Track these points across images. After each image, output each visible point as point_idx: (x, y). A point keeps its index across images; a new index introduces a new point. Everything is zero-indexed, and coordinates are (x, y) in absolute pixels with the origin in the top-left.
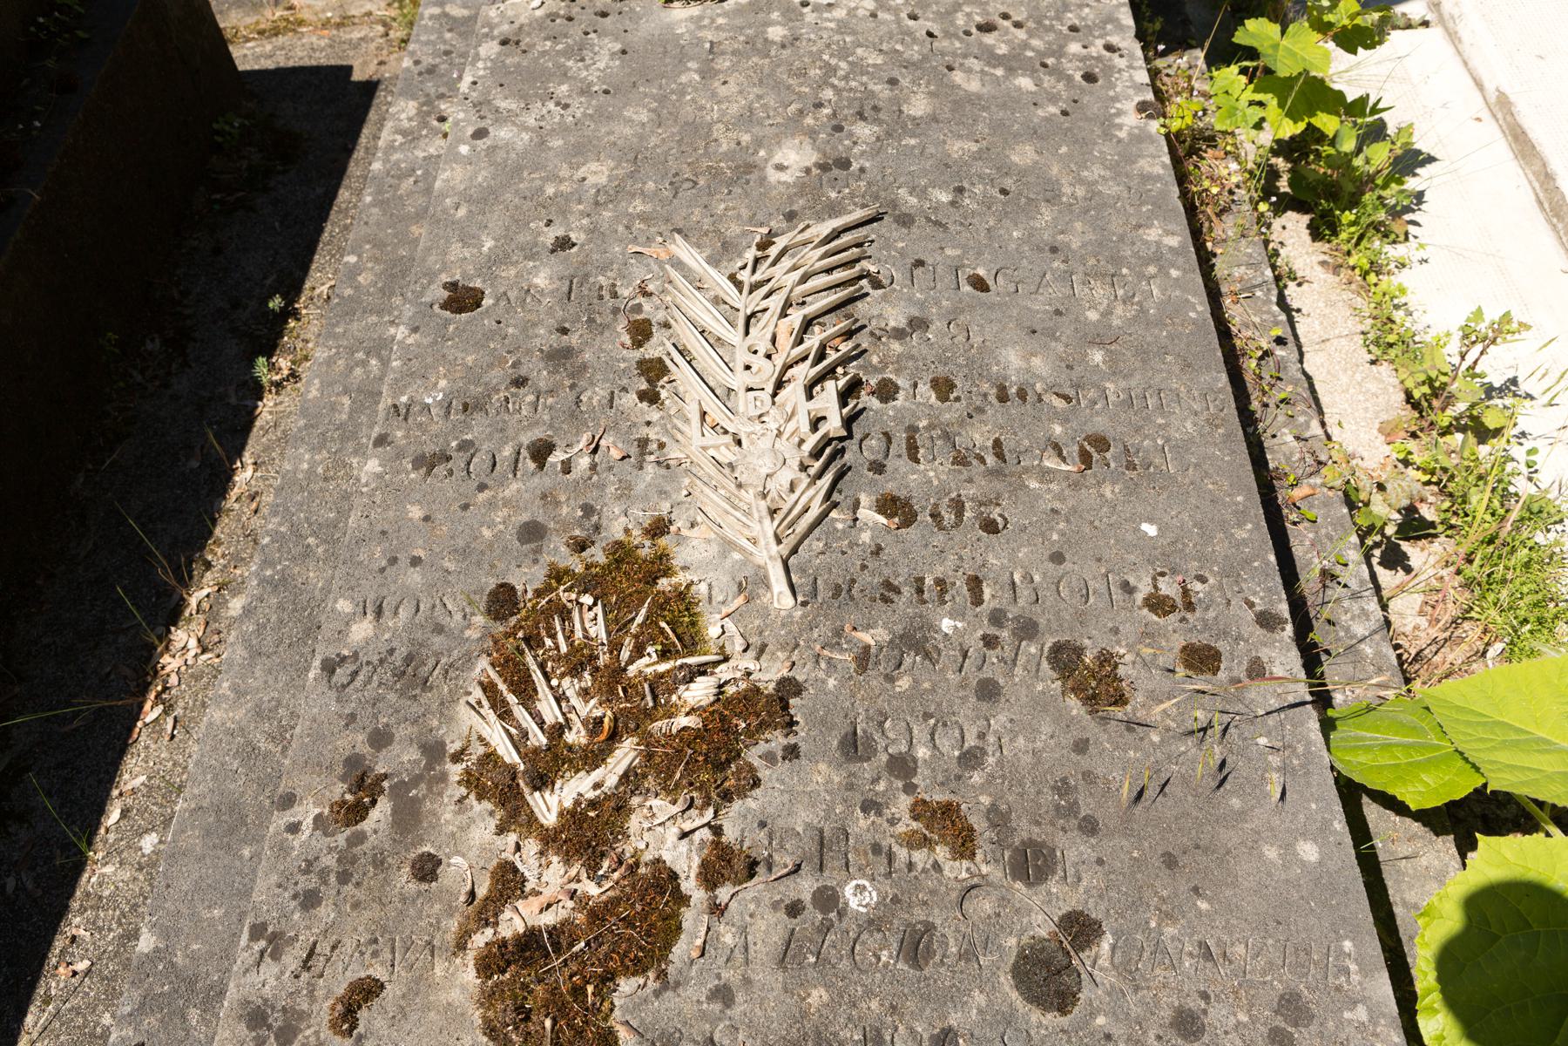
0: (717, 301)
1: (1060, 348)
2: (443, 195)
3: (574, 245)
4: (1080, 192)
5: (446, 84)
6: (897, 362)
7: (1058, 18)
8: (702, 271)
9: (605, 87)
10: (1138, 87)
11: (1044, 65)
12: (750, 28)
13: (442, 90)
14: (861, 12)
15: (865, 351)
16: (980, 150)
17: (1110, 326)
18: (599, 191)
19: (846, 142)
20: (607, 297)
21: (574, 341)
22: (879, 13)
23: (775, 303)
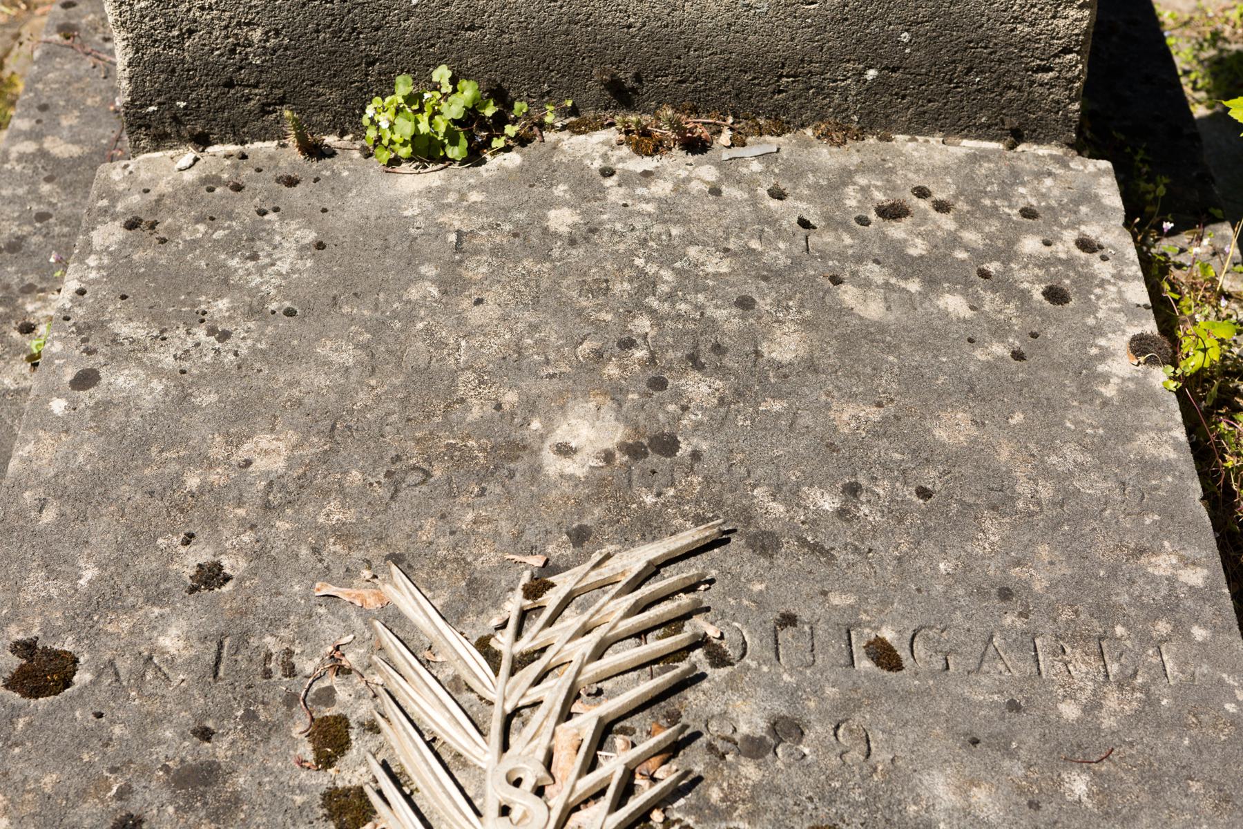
0: (456, 687)
1: (1019, 771)
2: (19, 485)
3: (227, 579)
4: (1046, 491)
5: (38, 269)
6: (752, 799)
7: (1005, 196)
8: (433, 632)
9: (287, 304)
10: (1132, 311)
11: (984, 274)
12: (520, 210)
13: (31, 278)
14: (695, 186)
15: (699, 779)
16: (885, 419)
17: (1098, 729)
18: (271, 484)
19: (671, 408)
20: (278, 674)
21: (220, 753)
22: (723, 188)
23: (553, 692)
